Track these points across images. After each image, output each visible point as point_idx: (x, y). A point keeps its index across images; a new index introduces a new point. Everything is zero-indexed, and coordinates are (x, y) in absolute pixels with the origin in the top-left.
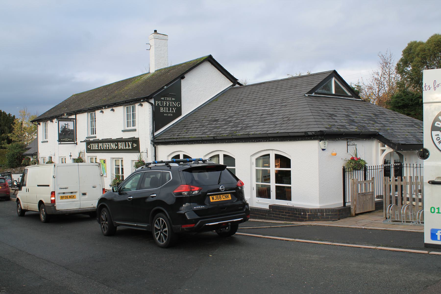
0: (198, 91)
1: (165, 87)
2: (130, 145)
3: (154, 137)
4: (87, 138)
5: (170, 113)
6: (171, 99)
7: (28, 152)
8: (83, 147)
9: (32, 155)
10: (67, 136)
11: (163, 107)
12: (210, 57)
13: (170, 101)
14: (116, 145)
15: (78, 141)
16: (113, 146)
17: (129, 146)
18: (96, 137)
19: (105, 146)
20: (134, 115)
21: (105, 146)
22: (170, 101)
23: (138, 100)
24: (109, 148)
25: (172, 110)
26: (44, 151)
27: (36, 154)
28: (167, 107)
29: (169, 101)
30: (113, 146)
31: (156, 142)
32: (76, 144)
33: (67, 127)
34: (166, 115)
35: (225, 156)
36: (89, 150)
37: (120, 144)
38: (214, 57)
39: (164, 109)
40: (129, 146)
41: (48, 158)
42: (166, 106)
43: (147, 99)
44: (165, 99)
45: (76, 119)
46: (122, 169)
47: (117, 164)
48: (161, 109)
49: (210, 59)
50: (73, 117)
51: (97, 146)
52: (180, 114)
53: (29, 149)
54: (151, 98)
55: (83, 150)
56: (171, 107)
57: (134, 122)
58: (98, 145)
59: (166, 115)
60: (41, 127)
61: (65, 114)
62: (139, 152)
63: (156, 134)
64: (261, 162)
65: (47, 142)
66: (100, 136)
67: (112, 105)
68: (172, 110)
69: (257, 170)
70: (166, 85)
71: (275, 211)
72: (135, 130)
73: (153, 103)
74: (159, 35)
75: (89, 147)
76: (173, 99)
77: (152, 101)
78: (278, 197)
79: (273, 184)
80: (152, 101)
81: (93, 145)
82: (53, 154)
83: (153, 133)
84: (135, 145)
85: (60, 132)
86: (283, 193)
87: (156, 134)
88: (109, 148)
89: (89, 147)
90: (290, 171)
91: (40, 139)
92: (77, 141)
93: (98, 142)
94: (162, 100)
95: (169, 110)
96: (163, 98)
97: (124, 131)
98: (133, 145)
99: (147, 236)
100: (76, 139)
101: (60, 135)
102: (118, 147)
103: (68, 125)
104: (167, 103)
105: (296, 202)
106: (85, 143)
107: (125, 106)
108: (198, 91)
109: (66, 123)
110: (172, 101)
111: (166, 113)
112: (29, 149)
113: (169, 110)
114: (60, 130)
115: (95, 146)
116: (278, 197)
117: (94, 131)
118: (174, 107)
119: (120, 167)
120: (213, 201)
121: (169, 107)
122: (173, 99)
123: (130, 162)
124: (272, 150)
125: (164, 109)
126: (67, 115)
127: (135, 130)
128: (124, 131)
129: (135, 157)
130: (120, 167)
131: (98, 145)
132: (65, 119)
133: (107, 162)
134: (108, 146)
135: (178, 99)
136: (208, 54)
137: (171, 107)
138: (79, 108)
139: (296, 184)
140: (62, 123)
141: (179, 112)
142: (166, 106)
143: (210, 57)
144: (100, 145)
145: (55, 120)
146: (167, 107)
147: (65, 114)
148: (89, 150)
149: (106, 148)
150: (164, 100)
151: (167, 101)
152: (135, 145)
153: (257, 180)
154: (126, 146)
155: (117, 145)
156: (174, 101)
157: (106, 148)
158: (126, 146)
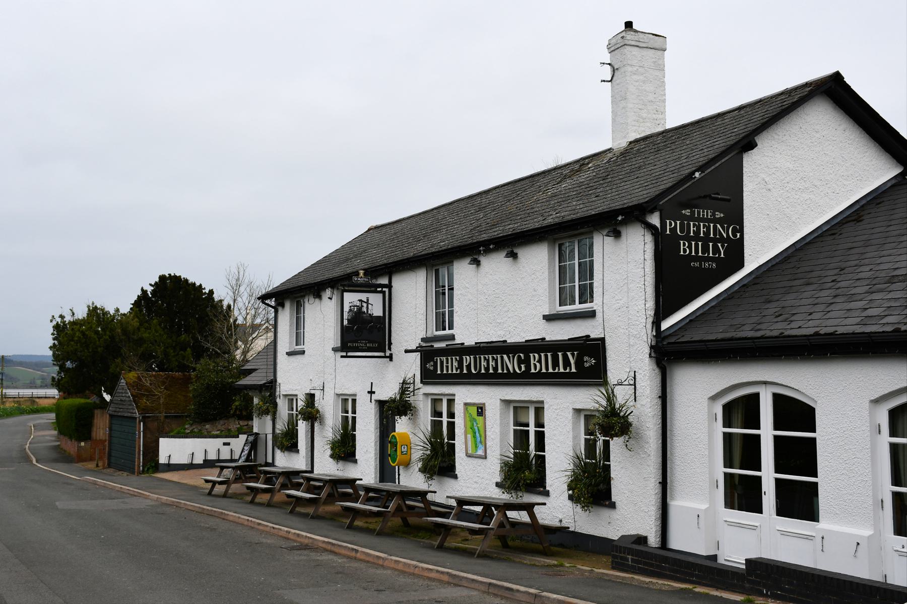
0: (795, 192)
1: (697, 175)
2: (572, 361)
3: (659, 335)
4: (423, 340)
5: (709, 259)
6: (713, 214)
8: (411, 366)
9: (259, 388)
10: (365, 336)
11: (688, 239)
12: (837, 77)
13: (709, 221)
14: (520, 362)
15: (397, 348)
16: (512, 364)
17: (567, 363)
18: (452, 337)
19: (484, 363)
20: (587, 271)
21: (484, 363)
22: (709, 221)
23: (612, 222)
24: (496, 369)
25: (716, 250)
27: (271, 386)
28: (701, 239)
29: (705, 221)
30: (512, 364)
31: (669, 353)
32: (391, 358)
33: (364, 309)
34: (697, 264)
35: (777, 398)
36: (428, 376)
37: (534, 358)
38: (848, 80)
39: (690, 247)
40: (567, 363)
41: (303, 398)
42: (697, 237)
43: (635, 214)
44: (693, 213)
45: (390, 286)
46: (540, 437)
47: (523, 420)
48: (683, 246)
49: (835, 91)
50: (385, 281)
51: (455, 364)
52: (740, 265)
53: (250, 371)
54: (652, 212)
55: (410, 375)
56: (711, 240)
58: (460, 363)
59: (697, 264)
61: (362, 272)
62: (605, 383)
63: (665, 325)
64: (738, 417)
65: (303, 352)
66: (466, 333)
67: (510, 244)
68: (716, 250)
69: (727, 438)
70: (701, 169)
72: (592, 314)
73: (658, 225)
74: (641, 35)
75: (430, 366)
76: (719, 215)
77: (655, 220)
79: (768, 475)
80: (655, 220)
81: (444, 361)
82: (318, 384)
83: (657, 323)
84: (589, 362)
85: (346, 322)
87: (665, 325)
88: (496, 369)
89: (430, 366)
91: (285, 343)
92: (393, 351)
93: (462, 351)
94: (683, 218)
95: (705, 249)
96: (687, 212)
97: (549, 318)
98: (586, 361)
100: (390, 344)
101: (345, 332)
102: (528, 367)
103: (367, 303)
104: (708, 228)
106: (419, 354)
107: (555, 241)
108: (795, 192)
109: (363, 296)
110: (715, 221)
111: (697, 258)
112: (250, 371)
113: (705, 249)
114: (345, 317)
115: (451, 365)
117: (444, 319)
118: (722, 240)
119: (532, 429)
121: (706, 240)
122: (719, 215)
123: (570, 414)
124: (765, 383)
125: (690, 247)
126: (365, 274)
127: (592, 314)
128: (549, 318)
129: (589, 398)
130: (532, 429)
131: (460, 363)
132: (361, 285)
133: (488, 412)
134: (492, 363)
135: (735, 216)
136: (825, 71)
137: (711, 240)
138: (399, 255)
140: (351, 299)
141: (735, 257)
142: (697, 237)
143: (837, 77)
144: (467, 359)
145: (328, 292)
146: (701, 239)
147: (362, 272)
148: (428, 376)
149: (487, 369)
150: (691, 218)
151: (700, 220)
152: (589, 362)
153: (728, 463)
154: (556, 364)
155: (527, 362)
156: (720, 221)
157: (487, 369)
158: (556, 364)
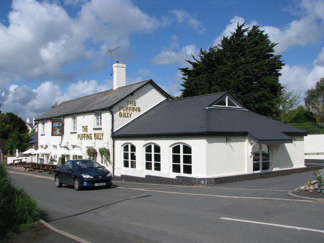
7: (185, 81)
12: (151, 80)
26: (41, 141)
53: (32, 139)
57: (101, 123)
60: (40, 125)
65: (44, 135)
71: (180, 180)
78: (185, 172)
79: (182, 164)
86: (188, 170)
90: (191, 156)
99: (72, 187)
105: (197, 173)
116: (185, 172)
120: (129, 172)
127: (101, 129)
128: (94, 129)
139: (194, 164)
143: (151, 80)
